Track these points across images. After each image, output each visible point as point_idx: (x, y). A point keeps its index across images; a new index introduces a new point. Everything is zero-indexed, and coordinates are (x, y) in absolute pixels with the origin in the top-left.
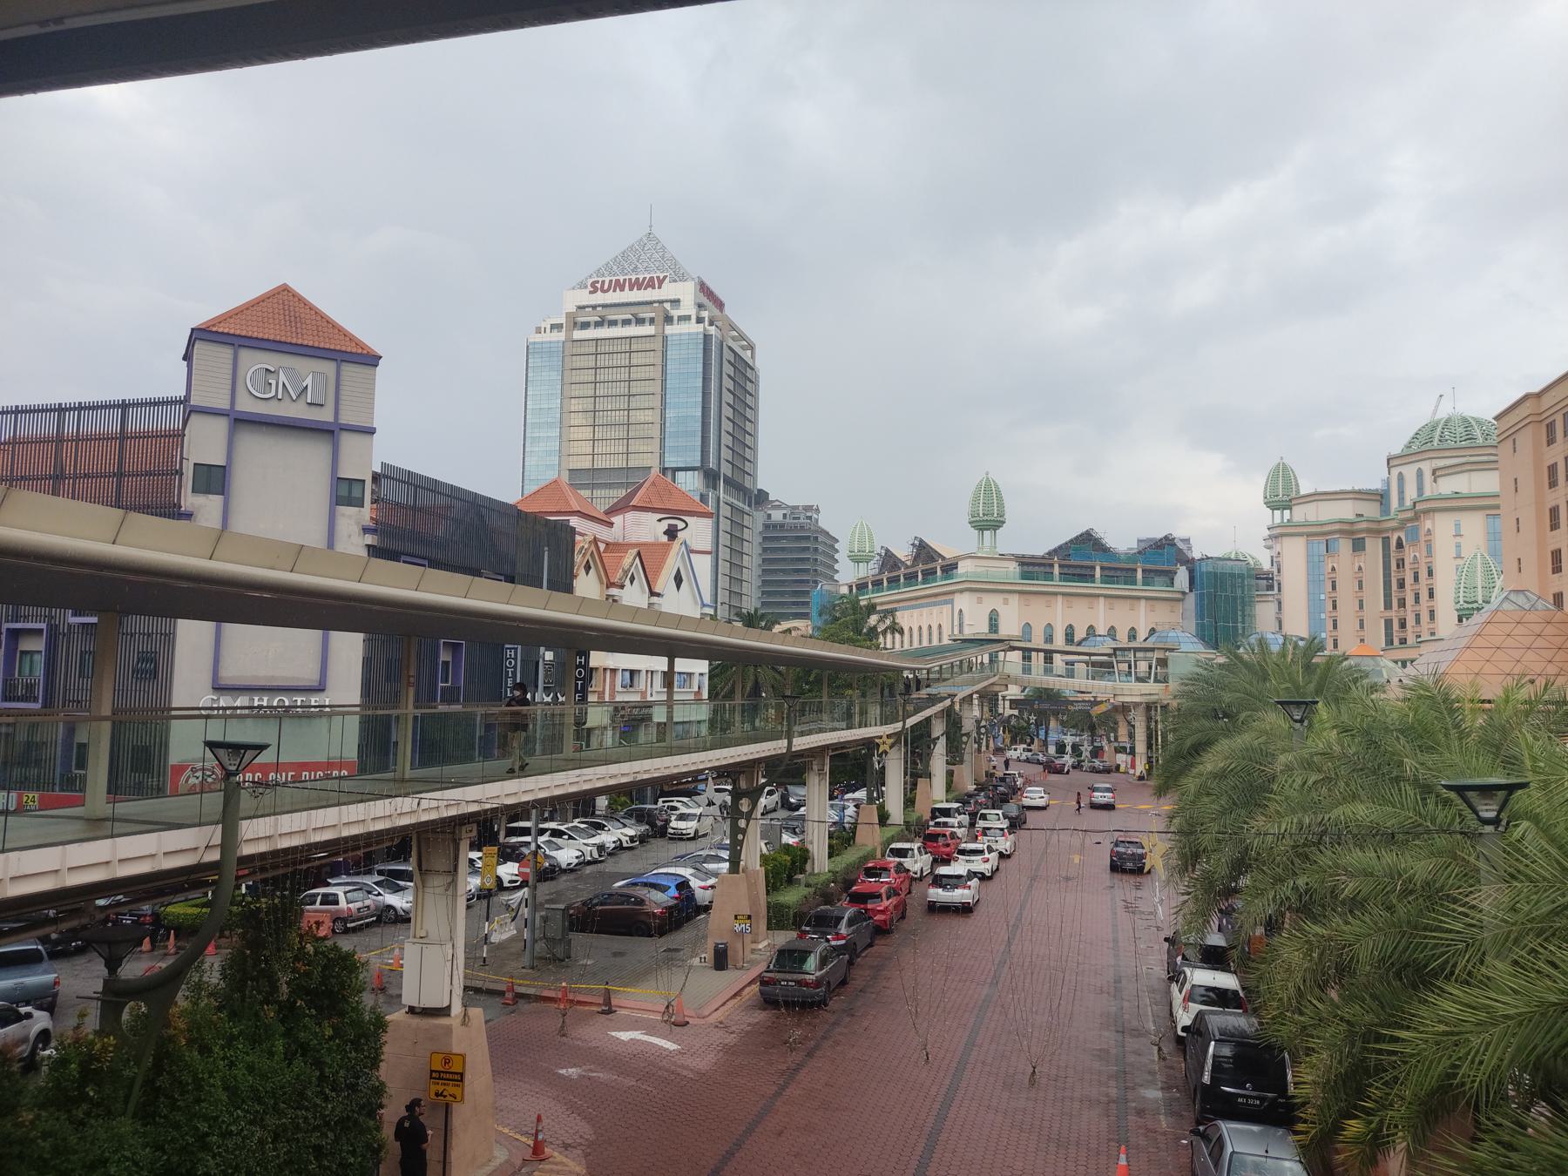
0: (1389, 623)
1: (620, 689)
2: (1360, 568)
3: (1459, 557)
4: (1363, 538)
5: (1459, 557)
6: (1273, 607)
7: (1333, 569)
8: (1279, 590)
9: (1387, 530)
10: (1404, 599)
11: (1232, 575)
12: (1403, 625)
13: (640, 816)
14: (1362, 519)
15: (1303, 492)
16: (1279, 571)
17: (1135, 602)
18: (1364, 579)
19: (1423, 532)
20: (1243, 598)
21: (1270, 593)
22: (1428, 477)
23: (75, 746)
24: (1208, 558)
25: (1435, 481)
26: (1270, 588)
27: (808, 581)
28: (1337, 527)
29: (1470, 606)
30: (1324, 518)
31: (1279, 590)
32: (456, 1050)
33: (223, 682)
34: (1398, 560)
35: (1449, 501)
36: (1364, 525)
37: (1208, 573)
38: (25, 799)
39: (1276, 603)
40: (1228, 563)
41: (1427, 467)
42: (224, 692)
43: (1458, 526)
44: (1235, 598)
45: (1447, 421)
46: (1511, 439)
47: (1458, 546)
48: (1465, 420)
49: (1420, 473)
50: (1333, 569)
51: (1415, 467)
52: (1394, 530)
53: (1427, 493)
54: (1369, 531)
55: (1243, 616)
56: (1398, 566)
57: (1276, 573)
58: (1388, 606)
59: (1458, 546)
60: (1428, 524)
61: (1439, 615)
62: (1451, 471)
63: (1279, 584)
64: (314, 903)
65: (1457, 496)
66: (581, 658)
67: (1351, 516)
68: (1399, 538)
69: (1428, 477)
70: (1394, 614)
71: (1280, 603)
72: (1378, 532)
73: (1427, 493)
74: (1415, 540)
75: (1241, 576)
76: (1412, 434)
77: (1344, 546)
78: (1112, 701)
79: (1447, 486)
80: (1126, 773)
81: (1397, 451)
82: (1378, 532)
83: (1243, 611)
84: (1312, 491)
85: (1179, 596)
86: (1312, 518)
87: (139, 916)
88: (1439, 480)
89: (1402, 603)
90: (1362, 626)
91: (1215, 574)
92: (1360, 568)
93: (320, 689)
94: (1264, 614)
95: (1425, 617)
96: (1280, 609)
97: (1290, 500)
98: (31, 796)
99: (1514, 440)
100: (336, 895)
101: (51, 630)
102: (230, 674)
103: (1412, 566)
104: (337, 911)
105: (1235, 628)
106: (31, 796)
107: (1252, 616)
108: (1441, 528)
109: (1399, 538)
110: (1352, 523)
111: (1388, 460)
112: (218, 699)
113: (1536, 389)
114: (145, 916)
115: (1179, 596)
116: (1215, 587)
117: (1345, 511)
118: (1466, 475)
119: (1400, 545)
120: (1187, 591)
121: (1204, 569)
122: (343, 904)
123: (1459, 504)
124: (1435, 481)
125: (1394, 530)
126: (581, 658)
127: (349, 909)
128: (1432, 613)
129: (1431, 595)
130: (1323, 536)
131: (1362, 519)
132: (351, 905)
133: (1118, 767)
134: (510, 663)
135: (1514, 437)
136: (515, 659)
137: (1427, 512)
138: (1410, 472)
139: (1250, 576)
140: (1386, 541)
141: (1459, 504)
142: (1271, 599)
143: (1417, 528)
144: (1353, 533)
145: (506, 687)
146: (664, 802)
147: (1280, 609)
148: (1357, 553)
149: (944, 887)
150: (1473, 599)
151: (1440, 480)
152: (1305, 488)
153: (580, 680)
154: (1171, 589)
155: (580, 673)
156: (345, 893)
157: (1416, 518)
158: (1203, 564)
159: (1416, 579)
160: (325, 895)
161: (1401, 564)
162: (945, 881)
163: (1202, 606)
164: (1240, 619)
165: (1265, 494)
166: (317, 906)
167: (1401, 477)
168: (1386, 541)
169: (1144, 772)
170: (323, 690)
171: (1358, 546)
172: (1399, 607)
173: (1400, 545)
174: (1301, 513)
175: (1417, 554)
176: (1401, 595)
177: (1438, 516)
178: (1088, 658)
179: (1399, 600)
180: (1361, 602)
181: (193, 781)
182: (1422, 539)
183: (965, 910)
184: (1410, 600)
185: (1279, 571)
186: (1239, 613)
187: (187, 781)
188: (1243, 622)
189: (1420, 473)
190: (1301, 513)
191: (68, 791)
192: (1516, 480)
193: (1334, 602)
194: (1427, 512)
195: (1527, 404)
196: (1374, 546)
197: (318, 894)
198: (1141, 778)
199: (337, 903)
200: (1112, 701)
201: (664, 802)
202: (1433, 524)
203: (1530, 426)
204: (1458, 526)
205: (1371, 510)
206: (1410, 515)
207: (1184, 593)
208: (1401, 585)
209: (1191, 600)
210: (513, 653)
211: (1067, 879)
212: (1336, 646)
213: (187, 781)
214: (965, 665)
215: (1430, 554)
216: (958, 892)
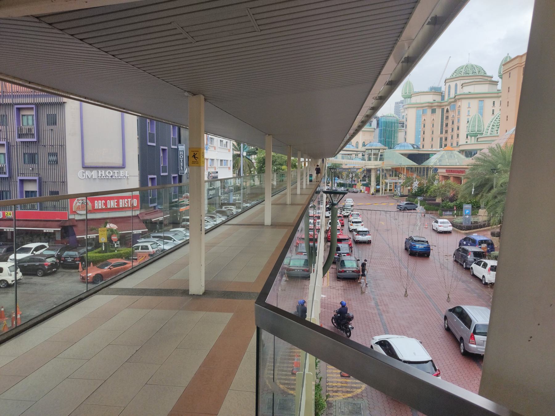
0: (441, 139)
1: (210, 167)
2: (433, 120)
3: (469, 115)
4: (435, 109)
5: (469, 115)
6: (404, 133)
7: (425, 120)
8: (406, 127)
9: (443, 106)
10: (447, 130)
11: (392, 123)
12: (446, 139)
13: (223, 213)
14: (435, 102)
16: (406, 121)
18: (434, 123)
19: (457, 106)
20: (394, 131)
21: (403, 128)
22: (459, 87)
23: (24, 192)
24: (384, 116)
25: (462, 88)
26: (403, 127)
27: (21, 129)
28: (427, 105)
29: (473, 133)
30: (422, 101)
31: (406, 127)
33: (86, 165)
34: (446, 116)
35: (466, 95)
36: (436, 104)
37: (384, 122)
38: (6, 214)
40: (391, 118)
41: (459, 83)
42: (87, 169)
43: (469, 104)
44: (392, 131)
45: (467, 66)
46: (508, 73)
47: (469, 111)
48: (472, 66)
49: (456, 85)
50: (425, 120)
51: (454, 83)
52: (446, 106)
53: (458, 93)
54: (437, 106)
55: (394, 137)
56: (446, 119)
57: (405, 121)
58: (442, 133)
59: (469, 111)
60: (459, 103)
61: (460, 136)
62: (468, 84)
63: (406, 125)
64: (138, 249)
65: (470, 93)
67: (431, 101)
68: (447, 109)
69: (459, 87)
70: (443, 136)
71: (406, 132)
72: (440, 106)
73: (458, 93)
74: (454, 110)
75: (394, 123)
76: (454, 70)
77: (429, 111)
78: (364, 168)
79: (467, 90)
80: (364, 193)
82: (440, 106)
83: (394, 135)
85: (373, 130)
86: (418, 101)
87: (74, 258)
88: (464, 88)
89: (446, 132)
90: (432, 140)
91: (386, 122)
92: (433, 120)
93: (123, 167)
94: (401, 136)
96: (406, 134)
97: (411, 95)
98: (9, 213)
99: (510, 73)
100: (147, 246)
101: (9, 144)
102: (89, 161)
103: (452, 119)
104: (149, 252)
105: (391, 141)
106: (9, 213)
107: (397, 137)
109: (447, 109)
110: (432, 103)
111: (446, 80)
112: (85, 172)
114: (77, 258)
115: (373, 130)
116: (386, 127)
117: (429, 98)
118: (473, 86)
119: (447, 111)
120: (376, 128)
121: (382, 120)
122: (151, 250)
123: (470, 96)
124: (462, 88)
125: (446, 106)
127: (153, 251)
128: (458, 135)
129: (458, 129)
131: (435, 102)
132: (153, 250)
133: (361, 191)
135: (509, 72)
136: (183, 155)
137: (459, 99)
138: (453, 85)
139: (397, 123)
140: (443, 110)
141: (470, 96)
142: (403, 131)
144: (432, 107)
145: (180, 166)
146: (225, 208)
147: (406, 134)
148: (433, 114)
149: (362, 235)
151: (464, 88)
154: (371, 127)
156: (151, 245)
157: (455, 101)
158: (382, 118)
159: (453, 123)
160: (142, 246)
161: (447, 118)
162: (361, 233)
163: (381, 133)
164: (393, 138)
166: (140, 250)
167: (449, 87)
168: (443, 110)
169: (374, 192)
170: (124, 168)
171: (433, 111)
172: (445, 133)
173: (447, 111)
174: (414, 100)
175: (454, 114)
176: (446, 129)
177: (463, 101)
178: (356, 152)
179: (445, 131)
180: (433, 132)
181: (78, 204)
182: (457, 109)
183: (369, 242)
184: (450, 131)
185: (406, 121)
186: (393, 136)
187: (76, 204)
188: (394, 139)
189: (456, 85)
190: (414, 100)
191: (32, 210)
192: (509, 88)
193: (424, 131)
194: (459, 99)
195: (517, 59)
196: (439, 111)
197: (140, 246)
198: (373, 194)
199: (148, 249)
200: (364, 168)
201: (225, 208)
202: (461, 104)
203: (517, 68)
204: (469, 104)
205: (438, 98)
206: (453, 100)
207: (375, 129)
208: (447, 125)
209: (377, 131)
210: (182, 153)
211: (388, 230)
212: (423, 147)
213: (76, 204)
214: (366, 157)
215: (459, 114)
216: (367, 237)
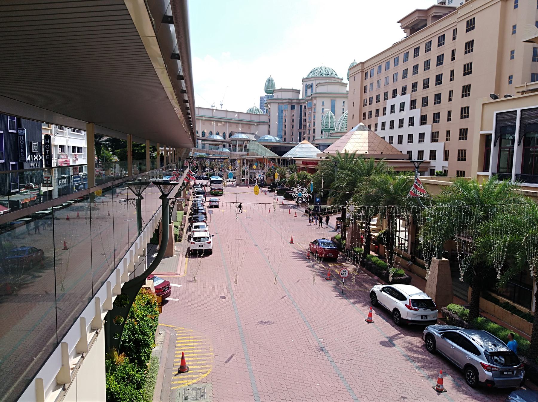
0: (300, 133)
4: (295, 105)
9: (301, 103)
15: (276, 88)
17: (238, 125)
28: (287, 101)
32: (307, 247)
39: (268, 126)
52: (304, 103)
58: (300, 128)
66: (47, 140)
67: (291, 98)
71: (269, 126)
76: (310, 71)
77: (289, 107)
78: (230, 158)
81: (305, 77)
84: (280, 88)
92: (293, 115)
95: (312, 132)
96: (269, 127)
108: (318, 102)
113: (363, 61)
126: (47, 140)
128: (314, 130)
130: (280, 102)
134: (22, 142)
135: (355, 76)
137: (315, 98)
140: (301, 107)
143: (311, 103)
147: (269, 127)
148: (293, 110)
150: (327, 126)
152: (277, 87)
153: (47, 149)
155: (47, 147)
157: (312, 99)
165: (265, 88)
171: (293, 107)
196: (297, 108)
210: (22, 138)
